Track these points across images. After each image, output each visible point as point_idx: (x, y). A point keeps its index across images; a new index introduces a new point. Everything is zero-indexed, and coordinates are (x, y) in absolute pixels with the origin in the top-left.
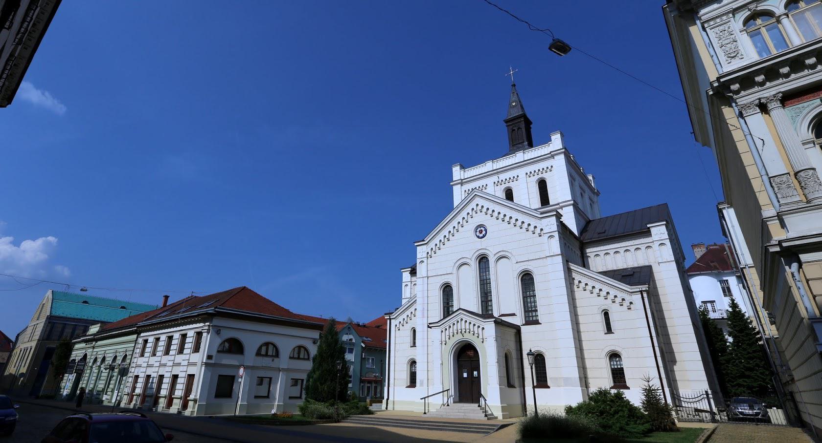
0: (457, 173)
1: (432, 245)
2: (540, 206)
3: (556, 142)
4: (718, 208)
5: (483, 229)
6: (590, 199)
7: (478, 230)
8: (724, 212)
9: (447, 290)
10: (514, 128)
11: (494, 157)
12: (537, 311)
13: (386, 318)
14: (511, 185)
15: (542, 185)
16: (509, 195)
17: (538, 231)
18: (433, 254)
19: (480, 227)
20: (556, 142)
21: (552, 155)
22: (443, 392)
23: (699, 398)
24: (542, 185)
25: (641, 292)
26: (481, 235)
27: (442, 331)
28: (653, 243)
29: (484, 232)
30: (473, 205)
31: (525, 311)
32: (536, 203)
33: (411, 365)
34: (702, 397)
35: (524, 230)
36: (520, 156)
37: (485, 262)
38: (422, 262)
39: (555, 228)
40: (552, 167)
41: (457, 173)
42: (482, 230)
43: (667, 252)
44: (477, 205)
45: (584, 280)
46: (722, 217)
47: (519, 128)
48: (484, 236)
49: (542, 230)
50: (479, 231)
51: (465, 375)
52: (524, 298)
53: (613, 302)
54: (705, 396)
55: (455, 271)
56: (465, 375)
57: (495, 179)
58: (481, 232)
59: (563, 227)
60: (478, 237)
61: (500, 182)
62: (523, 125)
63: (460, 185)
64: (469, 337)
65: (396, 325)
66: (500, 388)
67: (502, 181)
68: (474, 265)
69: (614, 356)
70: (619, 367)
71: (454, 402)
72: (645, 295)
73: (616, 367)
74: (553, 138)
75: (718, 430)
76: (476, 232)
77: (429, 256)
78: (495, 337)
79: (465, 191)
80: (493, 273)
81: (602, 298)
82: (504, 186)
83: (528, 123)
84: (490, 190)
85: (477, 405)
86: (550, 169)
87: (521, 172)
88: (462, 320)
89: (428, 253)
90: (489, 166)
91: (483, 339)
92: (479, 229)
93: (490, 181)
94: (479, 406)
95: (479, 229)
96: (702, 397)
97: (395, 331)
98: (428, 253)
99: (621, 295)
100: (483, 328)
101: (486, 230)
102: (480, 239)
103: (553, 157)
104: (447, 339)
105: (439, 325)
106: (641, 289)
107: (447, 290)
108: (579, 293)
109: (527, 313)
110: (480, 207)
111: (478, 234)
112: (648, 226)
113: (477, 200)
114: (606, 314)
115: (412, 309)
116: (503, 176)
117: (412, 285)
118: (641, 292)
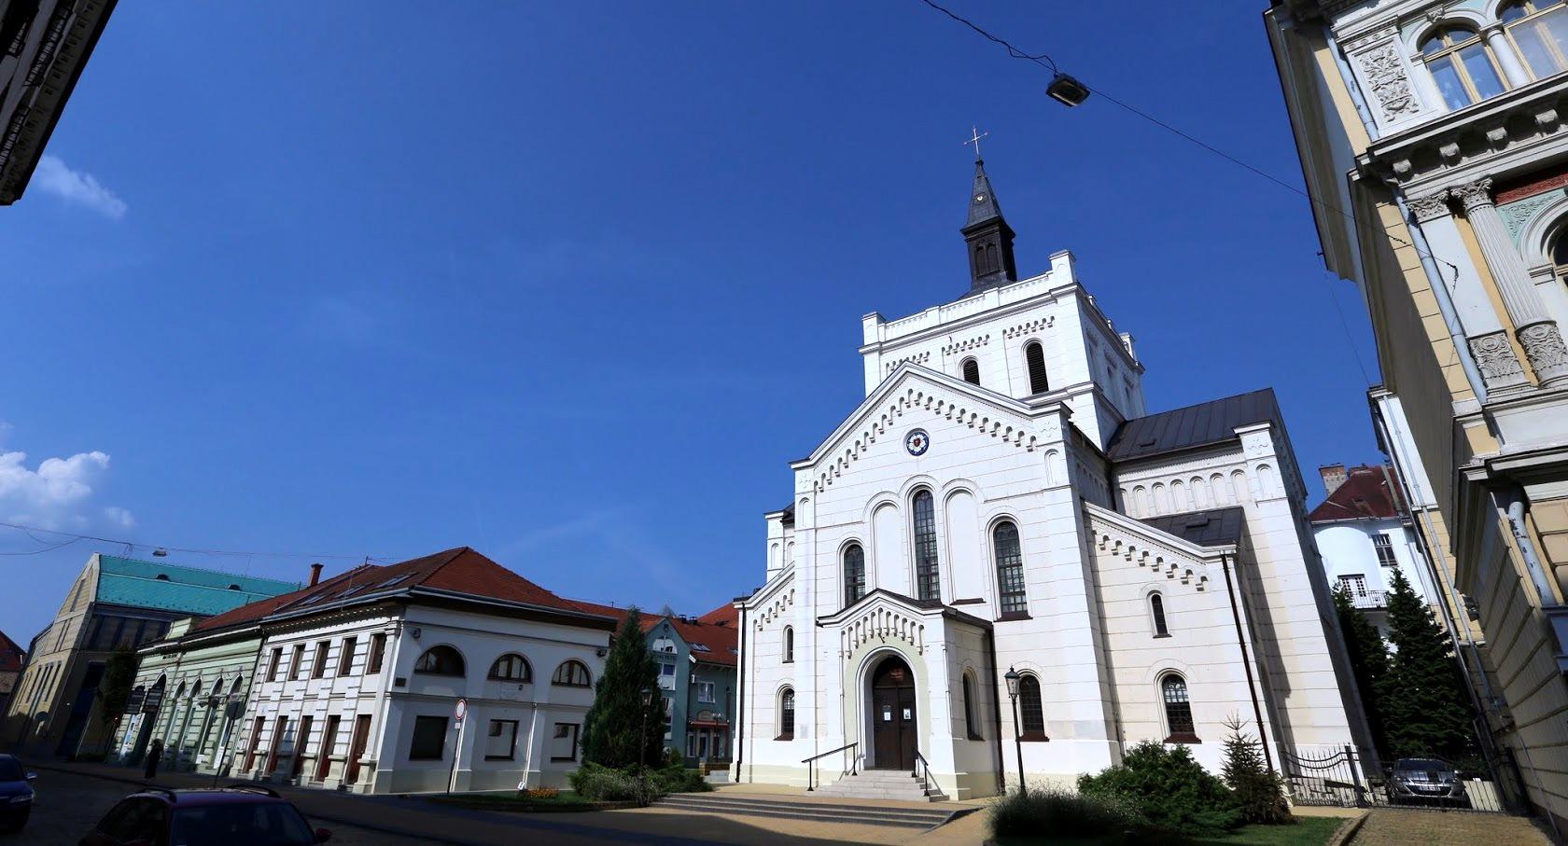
0: (872, 330)
1: (824, 467)
2: (1031, 394)
3: (1061, 272)
4: (1369, 397)
5: (921, 437)
6: (1126, 380)
7: (912, 440)
8: (1382, 404)
9: (853, 554)
10: (980, 245)
11: (942, 300)
12: (1024, 593)
13: (736, 607)
14: (975, 353)
15: (1035, 354)
16: (971, 372)
17: (1026, 441)
18: (826, 486)
19: (916, 434)
20: (1061, 272)
21: (1052, 296)
22: (845, 748)
23: (1334, 760)
24: (1035, 354)
25: (1223, 557)
26: (918, 449)
27: (843, 633)
28: (1245, 465)
29: (923, 444)
30: (902, 391)
31: (1002, 595)
32: (1023, 387)
33: (784, 698)
34: (1339, 757)
35: (999, 438)
36: (991, 299)
37: (925, 501)
38: (805, 500)
39: (1058, 435)
40: (1053, 318)
41: (872, 330)
42: (919, 440)
43: (1273, 482)
44: (911, 391)
45: (1115, 535)
46: (1377, 415)
47: (990, 245)
48: (923, 451)
49: (1033, 439)
50: (915, 440)
51: (887, 716)
52: (999, 568)
53: (1169, 577)
54: (1345, 756)
55: (867, 518)
56: (887, 716)
57: (943, 341)
58: (917, 443)
59: (1074, 436)
60: (912, 453)
61: (954, 347)
62: (997, 239)
63: (877, 354)
64: (894, 644)
65: (756, 621)
66: (953, 740)
67: (958, 345)
68: (904, 507)
69: (1172, 679)
70: (1181, 700)
71: (867, 768)
72: (1230, 563)
73: (1175, 700)
74: (1054, 263)
75: (1370, 820)
76: (909, 443)
77: (818, 490)
78: (943, 643)
79: (888, 365)
80: (941, 521)
81: (1148, 569)
82: (961, 356)
83: (1007, 234)
84: (935, 362)
85: (910, 773)
86: (1049, 322)
87: (994, 328)
88: (881, 610)
89: (816, 483)
90: (932, 317)
91: (921, 647)
92: (914, 437)
93: (934, 345)
94: (914, 775)
95: (914, 437)
96: (1339, 757)
97: (754, 632)
98: (816, 483)
99: (1184, 563)
100: (922, 627)
101: (927, 440)
102: (915, 457)
103: (1054, 299)
104: (853, 648)
105: (838, 620)
106: (1222, 553)
107: (853, 554)
108: (1104, 560)
109: (1005, 599)
110: (915, 396)
111: (912, 446)
112: (1237, 431)
113: (911, 383)
114: (1156, 600)
115: (786, 591)
116: (959, 337)
117: (787, 544)
118: (1223, 557)
